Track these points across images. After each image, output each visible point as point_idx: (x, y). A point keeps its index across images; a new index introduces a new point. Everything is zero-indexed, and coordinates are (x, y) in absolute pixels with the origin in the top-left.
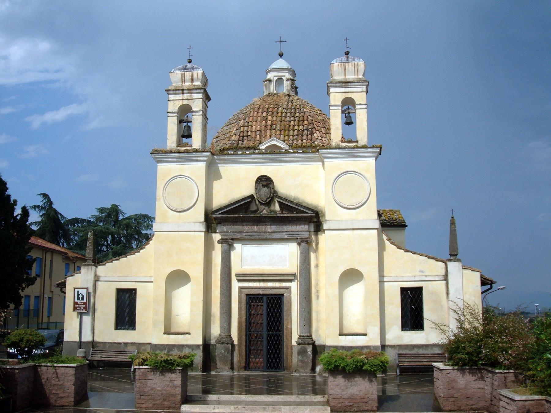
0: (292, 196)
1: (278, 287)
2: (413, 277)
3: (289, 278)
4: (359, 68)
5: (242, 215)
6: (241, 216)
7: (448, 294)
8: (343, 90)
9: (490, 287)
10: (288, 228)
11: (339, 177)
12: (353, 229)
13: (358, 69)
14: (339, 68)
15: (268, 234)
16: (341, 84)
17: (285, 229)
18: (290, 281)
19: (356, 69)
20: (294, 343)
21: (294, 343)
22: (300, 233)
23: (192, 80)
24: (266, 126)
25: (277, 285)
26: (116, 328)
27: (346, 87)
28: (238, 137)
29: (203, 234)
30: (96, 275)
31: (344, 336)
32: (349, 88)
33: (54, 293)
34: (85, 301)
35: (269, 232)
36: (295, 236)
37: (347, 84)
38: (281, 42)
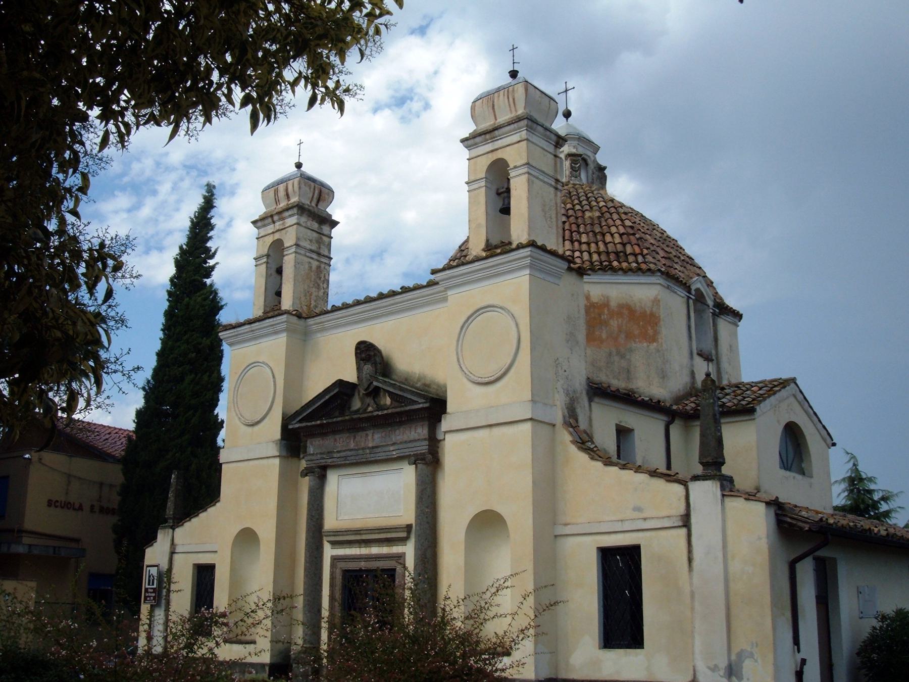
0: (415, 373)
1: (385, 554)
2: (620, 523)
4: (516, 95)
5: (325, 420)
6: (325, 422)
7: (690, 560)
8: (489, 147)
10: (398, 438)
11: (469, 322)
12: (490, 426)
13: (514, 99)
14: (484, 107)
15: (368, 451)
16: (483, 136)
17: (394, 439)
18: (403, 540)
19: (511, 99)
22: (410, 445)
23: (288, 196)
25: (385, 550)
27: (494, 139)
29: (277, 461)
30: (173, 544)
32: (498, 140)
34: (155, 586)
35: (369, 448)
36: (407, 452)
37: (493, 134)
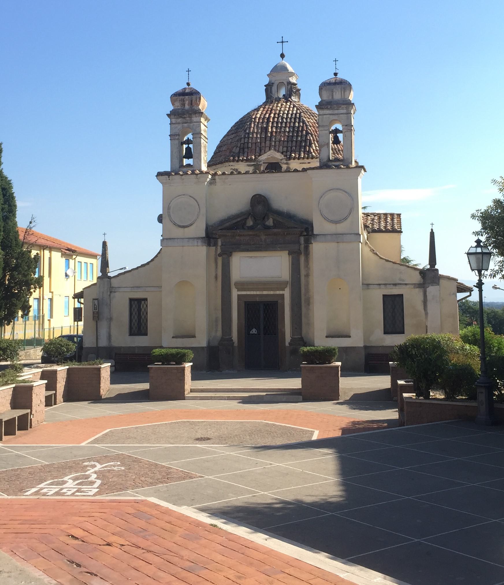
3: (281, 285)
9: (469, 294)
20: (287, 344)
21: (287, 344)
24: (266, 138)
26: (383, 295)
28: (238, 149)
31: (330, 338)
33: (54, 293)
38: (282, 42)
